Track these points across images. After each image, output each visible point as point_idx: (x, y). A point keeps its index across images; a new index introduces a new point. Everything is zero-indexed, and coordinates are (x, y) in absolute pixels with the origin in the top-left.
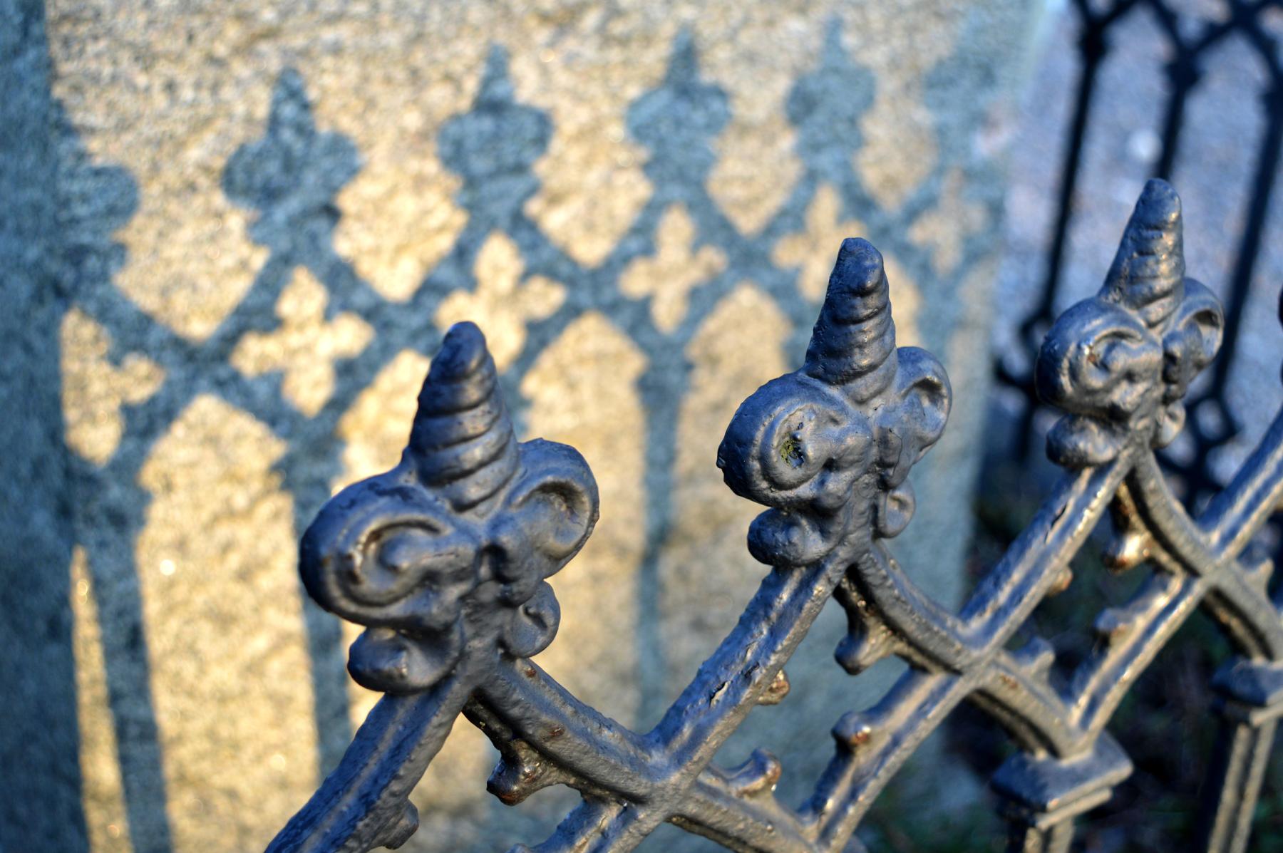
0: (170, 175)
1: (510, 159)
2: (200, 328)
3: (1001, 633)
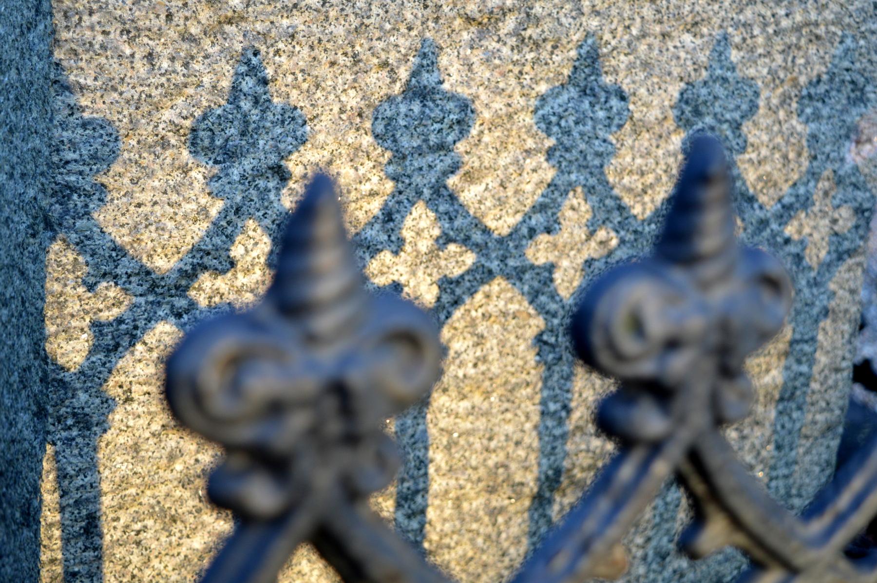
0: (145, 130)
1: (433, 139)
2: (164, 264)
3: (843, 536)
